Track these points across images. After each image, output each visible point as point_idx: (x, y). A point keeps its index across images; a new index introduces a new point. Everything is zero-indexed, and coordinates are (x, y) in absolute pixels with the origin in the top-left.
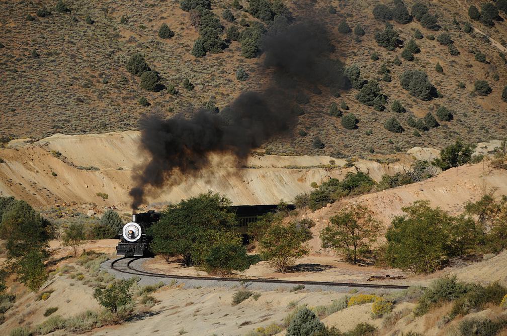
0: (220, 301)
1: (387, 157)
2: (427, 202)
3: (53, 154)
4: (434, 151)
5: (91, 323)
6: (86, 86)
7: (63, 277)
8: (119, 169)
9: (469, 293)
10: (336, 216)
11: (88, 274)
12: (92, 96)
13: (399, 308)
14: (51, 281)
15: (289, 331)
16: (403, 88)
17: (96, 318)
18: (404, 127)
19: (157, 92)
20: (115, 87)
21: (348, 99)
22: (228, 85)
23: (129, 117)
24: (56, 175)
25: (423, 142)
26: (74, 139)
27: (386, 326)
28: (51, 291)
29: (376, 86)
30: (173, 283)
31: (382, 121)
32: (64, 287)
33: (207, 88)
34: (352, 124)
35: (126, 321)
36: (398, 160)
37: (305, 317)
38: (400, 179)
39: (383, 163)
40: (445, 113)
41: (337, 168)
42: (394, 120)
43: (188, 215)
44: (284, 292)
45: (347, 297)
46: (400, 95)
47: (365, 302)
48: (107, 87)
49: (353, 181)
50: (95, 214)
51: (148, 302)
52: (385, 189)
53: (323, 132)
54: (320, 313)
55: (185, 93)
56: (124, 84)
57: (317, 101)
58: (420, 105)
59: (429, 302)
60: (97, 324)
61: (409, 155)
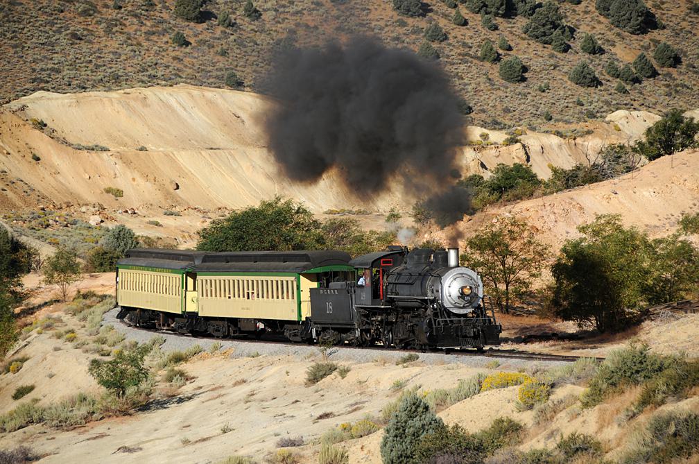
0: (287, 378)
1: (573, 126)
2: (617, 217)
3: (33, 124)
4: (649, 117)
5: (86, 414)
6: (85, 13)
7: (43, 336)
8: (141, 150)
9: (666, 372)
10: (477, 236)
11: (83, 330)
12: (95, 30)
13: (560, 394)
14: (25, 343)
15: (388, 431)
16: (600, 14)
17: (93, 404)
18: (601, 78)
19: (201, 23)
20: (132, 15)
21: (511, 32)
22: (315, 12)
23: (156, 64)
24: (38, 159)
25: (632, 102)
26: (66, 101)
27: (539, 423)
28: (24, 358)
29: (557, 12)
30: (216, 348)
31: (566, 69)
32: (45, 353)
33: (282, 16)
34: (516, 74)
35: (139, 410)
36: (589, 133)
37: (413, 409)
38: (581, 174)
39: (566, 136)
40: (669, 53)
41: (493, 146)
42: (584, 66)
43: (241, 238)
44: (386, 365)
45: (480, 376)
46: (595, 26)
47: (507, 385)
48: (119, 15)
49: (507, 179)
50: (102, 221)
51: (175, 378)
52: (557, 192)
53: (469, 88)
54: (439, 401)
55: (246, 24)
56: (147, 10)
57: (460, 37)
58: (628, 42)
59: (605, 386)
60: (95, 415)
61: (608, 123)
